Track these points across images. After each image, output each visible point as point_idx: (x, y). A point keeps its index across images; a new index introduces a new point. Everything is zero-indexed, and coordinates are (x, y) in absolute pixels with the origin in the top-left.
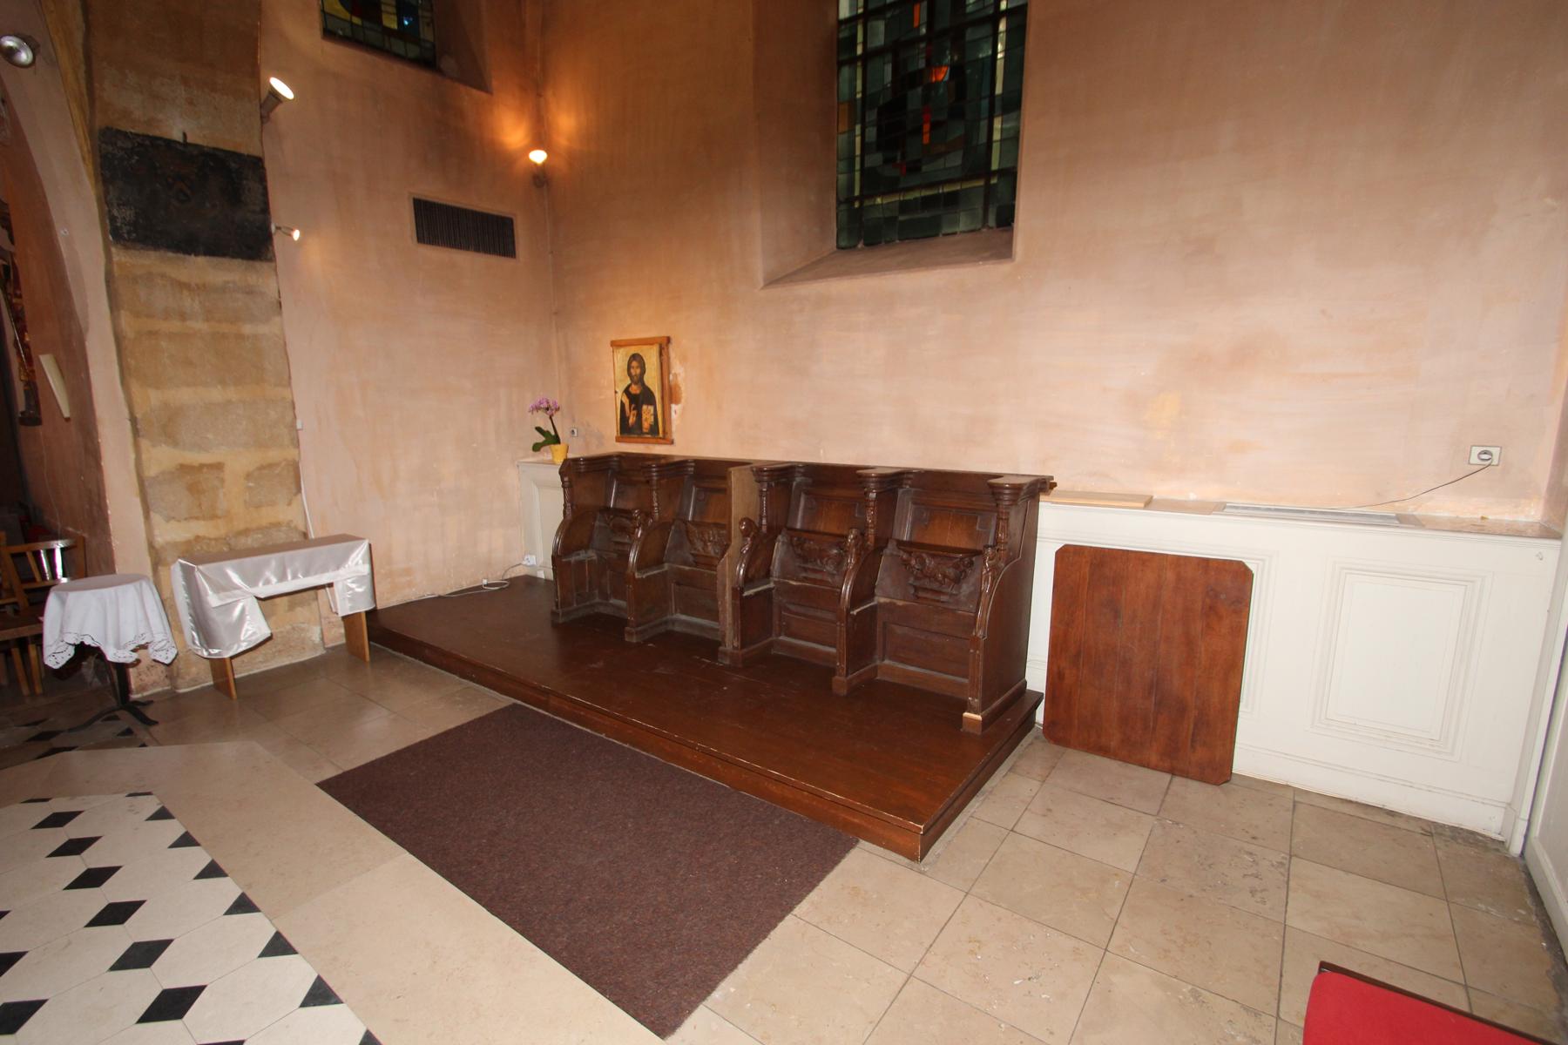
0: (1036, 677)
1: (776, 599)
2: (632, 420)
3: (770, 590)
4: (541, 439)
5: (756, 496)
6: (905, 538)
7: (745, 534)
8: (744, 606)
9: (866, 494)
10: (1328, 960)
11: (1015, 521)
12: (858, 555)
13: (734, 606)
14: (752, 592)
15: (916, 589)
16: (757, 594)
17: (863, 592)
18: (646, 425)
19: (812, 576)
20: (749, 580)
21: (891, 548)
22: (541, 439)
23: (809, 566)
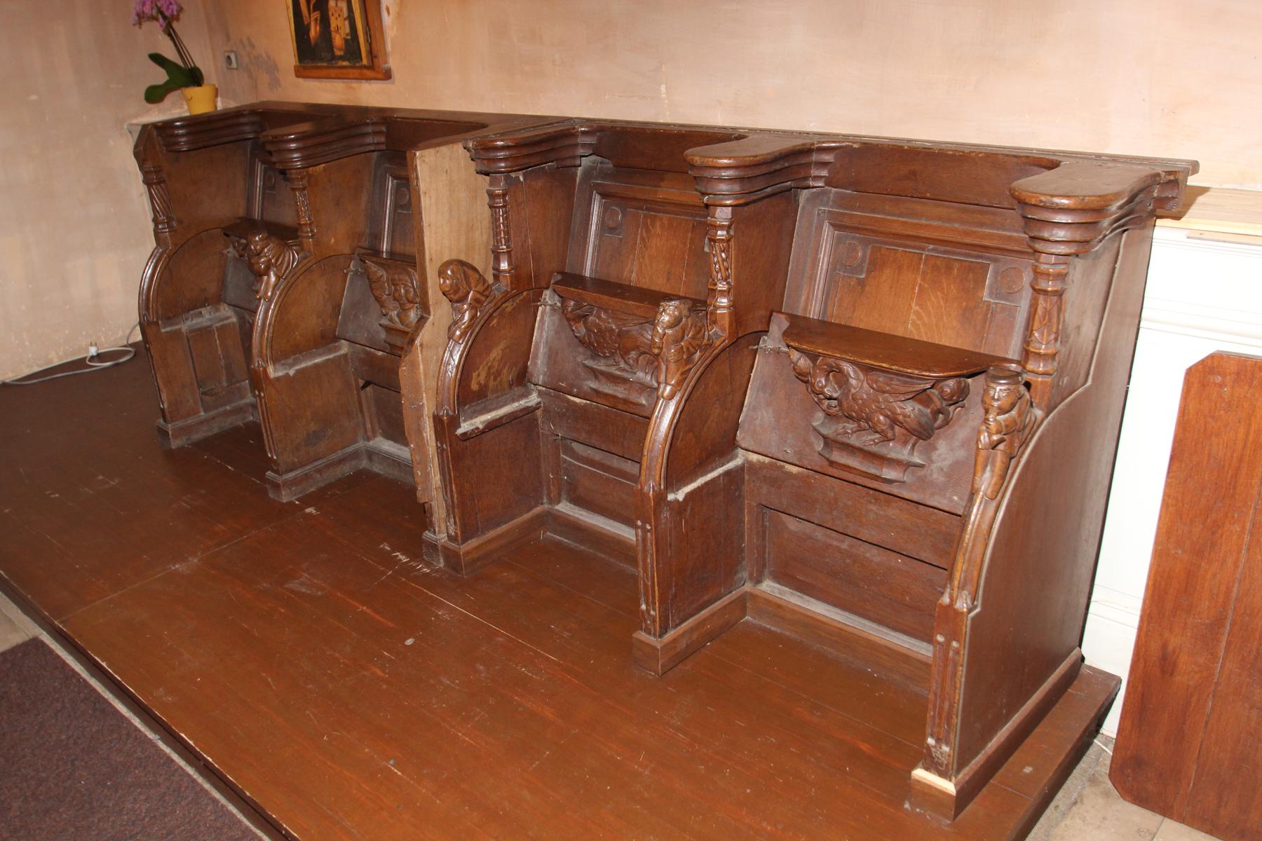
0: (1110, 637)
1: (545, 428)
2: (314, 31)
3: (529, 411)
4: (160, 76)
5: (482, 210)
6: (814, 312)
8: (459, 453)
11: (1082, 288)
13: (441, 452)
14: (480, 421)
15: (828, 442)
16: (492, 426)
17: (704, 438)
18: (338, 40)
19: (608, 389)
20: (467, 394)
22: (160, 76)
23: (601, 366)
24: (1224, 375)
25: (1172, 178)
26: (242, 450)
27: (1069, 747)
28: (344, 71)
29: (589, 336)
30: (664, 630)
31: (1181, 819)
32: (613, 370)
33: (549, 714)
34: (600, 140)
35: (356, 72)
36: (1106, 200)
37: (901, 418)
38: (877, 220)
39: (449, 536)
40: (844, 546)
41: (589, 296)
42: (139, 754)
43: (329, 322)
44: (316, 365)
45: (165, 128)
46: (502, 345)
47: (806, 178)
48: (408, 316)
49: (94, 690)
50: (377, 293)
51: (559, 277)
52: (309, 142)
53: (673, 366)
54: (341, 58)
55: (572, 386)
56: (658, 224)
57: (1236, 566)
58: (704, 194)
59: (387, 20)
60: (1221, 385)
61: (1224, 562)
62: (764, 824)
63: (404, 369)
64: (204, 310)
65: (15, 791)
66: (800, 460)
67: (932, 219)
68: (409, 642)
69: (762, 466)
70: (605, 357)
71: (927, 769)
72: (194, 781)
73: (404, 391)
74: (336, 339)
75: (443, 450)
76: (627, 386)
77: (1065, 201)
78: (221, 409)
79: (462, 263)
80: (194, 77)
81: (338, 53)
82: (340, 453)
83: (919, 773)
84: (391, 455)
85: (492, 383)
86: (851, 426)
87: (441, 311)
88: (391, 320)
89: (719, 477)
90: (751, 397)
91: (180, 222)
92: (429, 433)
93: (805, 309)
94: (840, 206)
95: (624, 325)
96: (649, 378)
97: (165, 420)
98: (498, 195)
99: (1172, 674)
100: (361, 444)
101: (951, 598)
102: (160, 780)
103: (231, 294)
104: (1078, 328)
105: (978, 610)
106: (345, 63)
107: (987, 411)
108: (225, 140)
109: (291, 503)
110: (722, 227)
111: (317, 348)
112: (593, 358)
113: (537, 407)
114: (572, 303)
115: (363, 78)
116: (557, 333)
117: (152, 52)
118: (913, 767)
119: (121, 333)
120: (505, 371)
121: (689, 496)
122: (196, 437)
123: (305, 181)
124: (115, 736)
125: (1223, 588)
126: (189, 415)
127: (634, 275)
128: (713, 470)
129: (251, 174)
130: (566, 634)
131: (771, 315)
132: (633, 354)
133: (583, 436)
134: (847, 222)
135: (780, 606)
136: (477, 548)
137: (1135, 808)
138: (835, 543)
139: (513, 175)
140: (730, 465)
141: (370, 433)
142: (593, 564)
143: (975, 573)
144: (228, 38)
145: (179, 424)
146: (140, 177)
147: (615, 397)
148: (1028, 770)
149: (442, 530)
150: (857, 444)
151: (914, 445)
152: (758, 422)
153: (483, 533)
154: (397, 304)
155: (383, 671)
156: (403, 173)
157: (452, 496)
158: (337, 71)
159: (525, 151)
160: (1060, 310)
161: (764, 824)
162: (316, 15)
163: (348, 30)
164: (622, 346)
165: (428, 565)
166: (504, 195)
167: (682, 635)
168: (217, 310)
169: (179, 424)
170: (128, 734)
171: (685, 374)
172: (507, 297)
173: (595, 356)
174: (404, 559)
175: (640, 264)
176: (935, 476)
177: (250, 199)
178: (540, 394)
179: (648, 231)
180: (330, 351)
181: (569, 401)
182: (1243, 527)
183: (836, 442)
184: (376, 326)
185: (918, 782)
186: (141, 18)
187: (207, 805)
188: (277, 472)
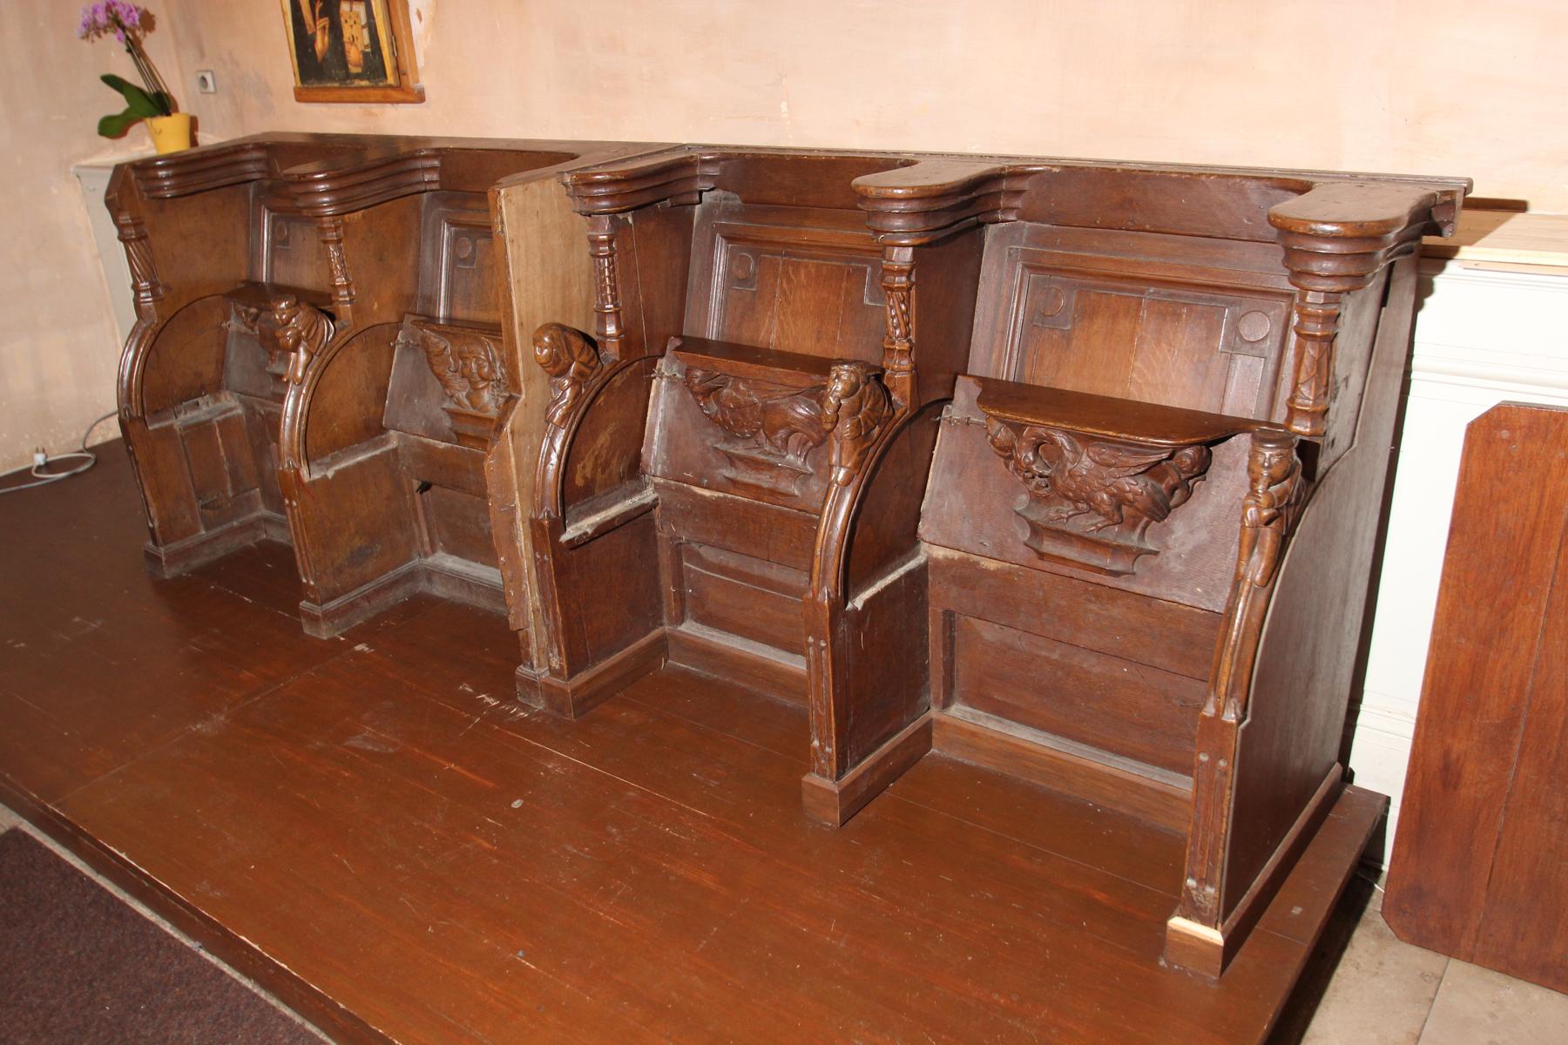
0: (1382, 757)
1: (665, 531)
2: (321, 43)
3: (646, 510)
4: (117, 104)
7: (555, 367)
8: (567, 567)
9: (882, 251)
10: (1519, 217)
12: (861, 436)
13: (540, 566)
15: (1037, 530)
16: (603, 530)
18: (354, 54)
19: (749, 477)
20: (573, 493)
21: (963, 403)
22: (117, 104)
23: (739, 449)
24: (1512, 430)
25: (1448, 198)
26: (265, 576)
27: (1340, 880)
28: (362, 92)
29: (723, 414)
30: (841, 770)
31: (1470, 958)
32: (755, 454)
33: (708, 881)
34: (724, 171)
35: (379, 93)
36: (1387, 225)
37: (1130, 496)
38: (1084, 259)
39: (552, 672)
40: (1055, 656)
41: (723, 364)
42: (176, 967)
43: (373, 409)
44: (360, 464)
45: (144, 168)
46: (610, 429)
47: (994, 211)
48: (480, 397)
49: (103, 890)
50: (439, 369)
51: (678, 343)
52: (345, 182)
53: (848, 445)
54: (358, 76)
55: (701, 476)
56: (802, 272)
57: (1531, 654)
58: (877, 232)
59: (417, 27)
60: (1510, 441)
61: (1516, 649)
62: (996, 997)
63: (490, 463)
64: (200, 400)
65: (18, 1024)
66: (1001, 553)
67: (1151, 255)
68: (517, 804)
69: (950, 563)
70: (744, 438)
71: (1186, 917)
72: (255, 996)
73: (491, 490)
74: (383, 430)
75: (544, 562)
76: (775, 473)
77: (1328, 228)
78: (225, 526)
79: (562, 328)
80: (162, 104)
81: (354, 70)
82: (391, 574)
83: (1177, 922)
84: (458, 573)
85: (600, 477)
86: (1067, 508)
87: (532, 391)
88: (459, 403)
89: (900, 579)
90: (934, 479)
91: (167, 288)
92: (523, 542)
93: (997, 371)
94: (1037, 244)
95: (770, 398)
96: (800, 462)
97: (155, 542)
98: (603, 242)
99: (1455, 788)
100: (416, 562)
101: (1218, 710)
102: (210, 998)
103: (235, 375)
104: (1346, 379)
105: (1248, 721)
106: (364, 83)
107: (1254, 481)
108: (218, 183)
109: (334, 641)
110: (900, 272)
111: (359, 442)
112: (726, 440)
113: (654, 504)
114: (699, 373)
115: (387, 100)
116: (677, 411)
117: (105, 73)
118: (1169, 915)
119: (74, 435)
120: (614, 461)
121: (868, 603)
122: (196, 562)
123: (341, 231)
124: (141, 946)
125: (1516, 681)
126: (185, 535)
127: (773, 336)
128: (893, 570)
129: (254, 226)
130: (713, 783)
131: (955, 379)
132: (782, 433)
133: (715, 538)
134: (1046, 262)
135: (974, 734)
136: (587, 683)
137: (1414, 949)
138: (1043, 653)
139: (621, 216)
140: (911, 565)
141: (428, 548)
142: (730, 699)
143: (1245, 677)
144: (202, 56)
145: (175, 546)
146: (115, 231)
147: (758, 487)
148: (1297, 911)
149: (543, 661)
150: (1075, 531)
151: (1144, 529)
152: (945, 509)
153: (594, 665)
154: (465, 382)
155: (491, 842)
156: (477, 219)
157: (555, 619)
158: (351, 93)
159: (637, 187)
160: (1329, 358)
161: (996, 997)
162: (324, 22)
163: (367, 41)
164: (767, 423)
165: (524, 707)
166: (610, 242)
167: (862, 776)
168: (217, 400)
169: (175, 546)
170: (158, 943)
171: (863, 454)
172: (617, 369)
173: (730, 437)
174: (493, 702)
175: (781, 323)
176: (1172, 564)
177: (253, 256)
178: (657, 487)
179: (789, 281)
180: (376, 447)
181: (695, 494)
182: (1539, 608)
183: (1048, 529)
184: (437, 411)
185: (1175, 931)
186: (93, 29)
187: (278, 1025)
188: (314, 601)
